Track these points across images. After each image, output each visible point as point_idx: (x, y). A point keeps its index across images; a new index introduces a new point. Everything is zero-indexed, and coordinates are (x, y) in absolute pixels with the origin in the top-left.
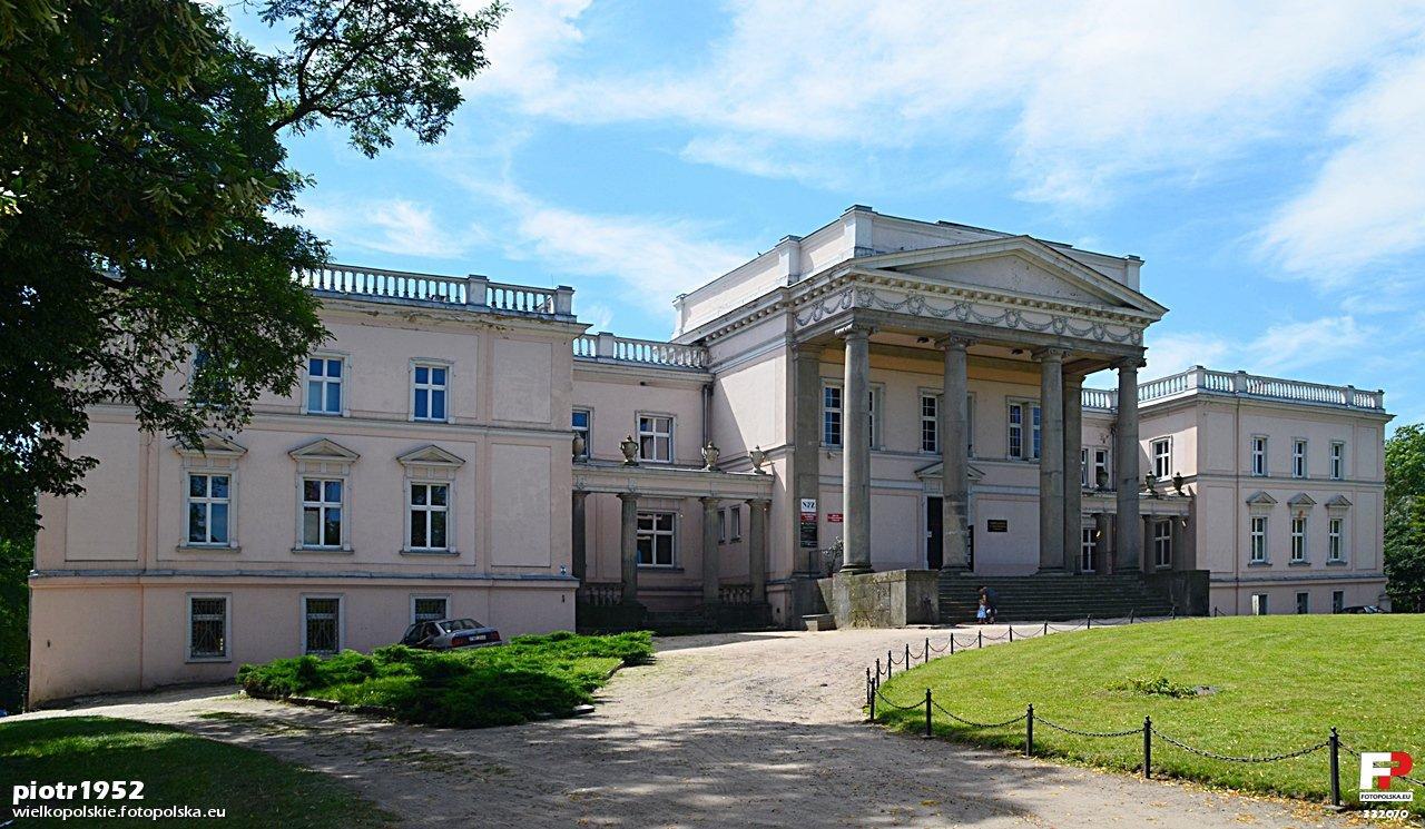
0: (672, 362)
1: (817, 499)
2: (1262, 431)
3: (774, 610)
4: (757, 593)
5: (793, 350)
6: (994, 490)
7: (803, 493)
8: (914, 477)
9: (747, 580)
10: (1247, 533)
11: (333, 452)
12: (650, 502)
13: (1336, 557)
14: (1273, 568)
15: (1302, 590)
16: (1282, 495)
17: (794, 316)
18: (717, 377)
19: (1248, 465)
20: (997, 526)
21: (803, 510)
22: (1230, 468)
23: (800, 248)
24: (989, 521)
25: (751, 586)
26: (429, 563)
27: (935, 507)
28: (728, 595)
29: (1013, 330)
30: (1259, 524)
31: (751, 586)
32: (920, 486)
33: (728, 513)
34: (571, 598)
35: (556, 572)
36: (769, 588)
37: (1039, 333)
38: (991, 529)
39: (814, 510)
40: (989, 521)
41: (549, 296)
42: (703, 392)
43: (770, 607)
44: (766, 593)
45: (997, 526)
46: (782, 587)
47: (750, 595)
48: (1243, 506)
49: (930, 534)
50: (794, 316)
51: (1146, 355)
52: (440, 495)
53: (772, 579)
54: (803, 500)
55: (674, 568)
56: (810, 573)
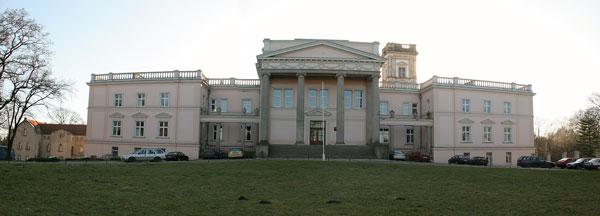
10: (460, 133)
11: (469, 121)
16: (128, 114)
19: (112, 103)
22: (451, 144)
26: (117, 139)
34: (198, 149)
35: (193, 142)
52: (166, 124)
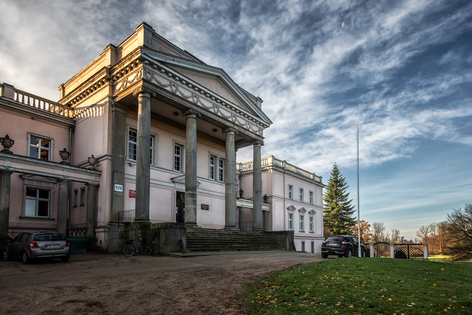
0: (62, 114)
1: (123, 186)
2: (291, 184)
3: (99, 242)
4: (90, 233)
5: (112, 106)
6: (204, 191)
7: (115, 181)
8: (170, 181)
9: (85, 226)
10: (287, 219)
12: (35, 182)
13: (291, 228)
14: (315, 234)
15: (303, 240)
17: (113, 87)
18: (77, 123)
19: (287, 196)
20: (205, 207)
21: (116, 190)
23: (117, 53)
24: (202, 205)
25: (86, 229)
27: (179, 195)
28: (72, 234)
29: (216, 114)
30: (291, 216)
31: (86, 229)
32: (173, 185)
33: (79, 192)
36: (96, 230)
37: (226, 119)
38: (202, 208)
39: (122, 191)
40: (202, 205)
41: (51, 105)
42: (69, 130)
43: (96, 240)
44: (95, 233)
45: (205, 207)
46: (102, 230)
47: (85, 233)
48: (286, 210)
49: (344, 257)
50: (113, 87)
51: (264, 140)
53: (98, 225)
54: (116, 185)
55: (49, 218)
56: (119, 223)
